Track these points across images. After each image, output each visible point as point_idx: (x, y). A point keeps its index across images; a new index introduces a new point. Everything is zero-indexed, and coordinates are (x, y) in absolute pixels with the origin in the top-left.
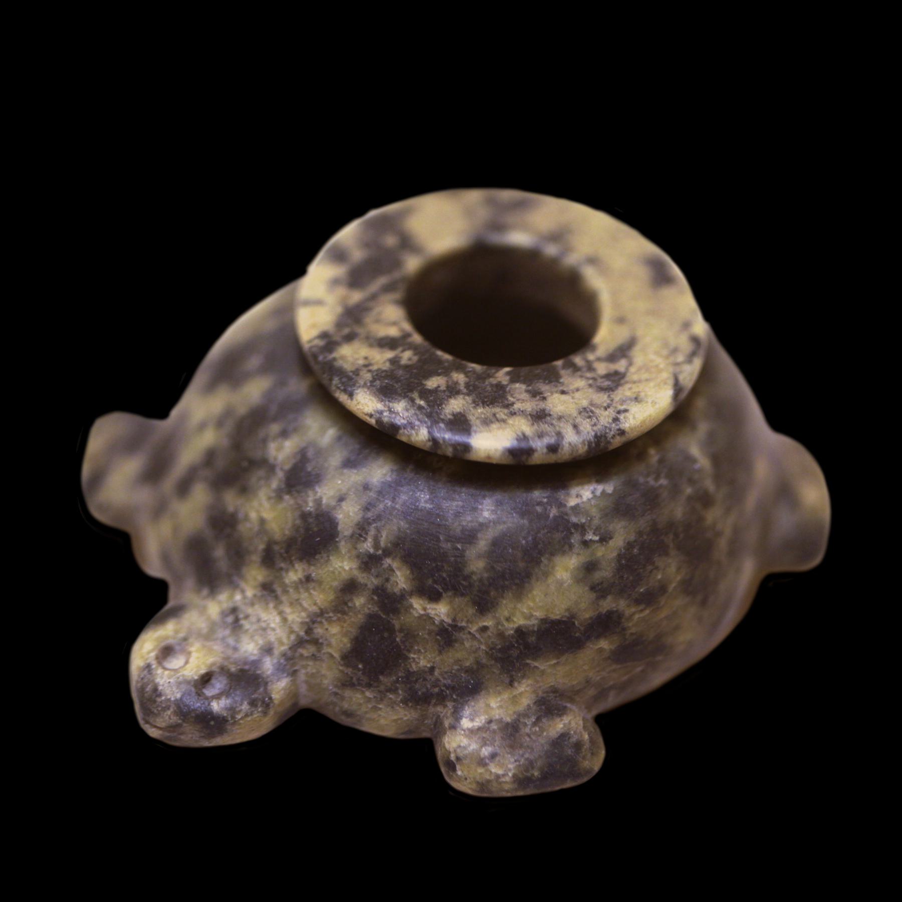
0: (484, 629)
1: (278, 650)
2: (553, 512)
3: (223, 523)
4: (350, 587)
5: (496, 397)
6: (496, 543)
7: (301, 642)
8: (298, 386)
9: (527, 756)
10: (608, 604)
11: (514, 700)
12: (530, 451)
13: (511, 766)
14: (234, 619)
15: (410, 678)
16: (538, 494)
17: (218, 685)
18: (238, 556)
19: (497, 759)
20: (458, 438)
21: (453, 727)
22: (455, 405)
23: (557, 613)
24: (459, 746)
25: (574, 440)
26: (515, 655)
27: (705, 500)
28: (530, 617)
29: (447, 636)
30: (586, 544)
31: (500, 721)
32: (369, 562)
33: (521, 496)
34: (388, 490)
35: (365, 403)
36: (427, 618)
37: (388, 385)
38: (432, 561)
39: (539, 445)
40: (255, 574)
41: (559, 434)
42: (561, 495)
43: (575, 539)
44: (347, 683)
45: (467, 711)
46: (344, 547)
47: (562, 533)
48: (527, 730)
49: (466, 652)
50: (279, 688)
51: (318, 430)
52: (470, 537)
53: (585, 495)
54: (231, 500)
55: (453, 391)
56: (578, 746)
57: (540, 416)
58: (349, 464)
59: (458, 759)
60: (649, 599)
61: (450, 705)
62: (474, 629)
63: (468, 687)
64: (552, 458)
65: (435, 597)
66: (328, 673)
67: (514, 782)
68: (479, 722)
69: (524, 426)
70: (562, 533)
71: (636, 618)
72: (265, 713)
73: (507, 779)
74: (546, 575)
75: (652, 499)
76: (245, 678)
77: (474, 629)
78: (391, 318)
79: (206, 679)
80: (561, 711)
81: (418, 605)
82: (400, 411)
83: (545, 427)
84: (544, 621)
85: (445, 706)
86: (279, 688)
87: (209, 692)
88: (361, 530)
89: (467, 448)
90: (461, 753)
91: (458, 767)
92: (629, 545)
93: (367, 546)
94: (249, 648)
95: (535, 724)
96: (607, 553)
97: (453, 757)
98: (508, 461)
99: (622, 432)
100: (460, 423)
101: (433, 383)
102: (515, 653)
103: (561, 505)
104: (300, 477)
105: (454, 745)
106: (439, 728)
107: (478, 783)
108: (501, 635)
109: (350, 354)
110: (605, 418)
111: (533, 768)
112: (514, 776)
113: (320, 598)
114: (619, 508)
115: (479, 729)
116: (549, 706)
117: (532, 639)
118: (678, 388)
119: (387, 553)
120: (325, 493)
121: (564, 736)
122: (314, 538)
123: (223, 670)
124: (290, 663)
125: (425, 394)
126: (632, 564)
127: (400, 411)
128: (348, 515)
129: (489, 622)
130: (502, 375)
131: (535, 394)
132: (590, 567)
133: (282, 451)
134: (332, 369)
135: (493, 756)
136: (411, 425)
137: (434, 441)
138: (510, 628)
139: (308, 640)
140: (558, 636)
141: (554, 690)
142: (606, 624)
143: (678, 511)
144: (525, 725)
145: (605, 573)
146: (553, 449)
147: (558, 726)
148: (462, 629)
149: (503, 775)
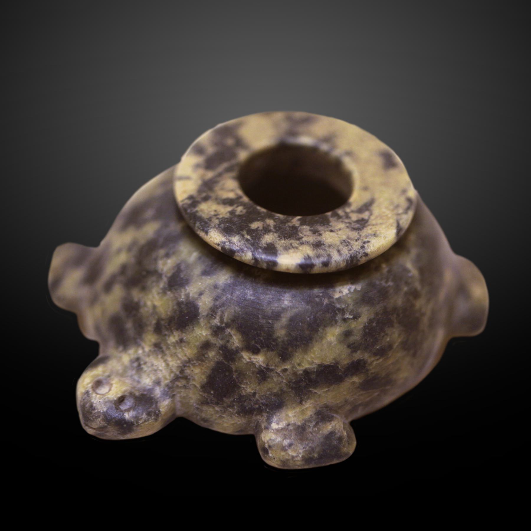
0: (285, 370)
1: (164, 383)
2: (326, 301)
3: (131, 308)
4: (206, 346)
5: (292, 234)
6: (292, 320)
7: (177, 378)
8: (175, 227)
9: (310, 445)
10: (358, 356)
11: (303, 412)
12: (312, 266)
13: (301, 451)
14: (138, 364)
15: (241, 399)
16: (317, 291)
17: (129, 403)
18: (140, 328)
19: (293, 447)
20: (270, 258)
21: (267, 428)
22: (268, 238)
23: (328, 361)
24: (270, 439)
25: (338, 259)
26: (303, 385)
27: (415, 294)
28: (312, 363)
29: (263, 374)
30: (345, 320)
31: (294, 424)
32: (217, 331)
33: (307, 292)
34: (229, 288)
35: (215, 237)
36: (252, 364)
37: (229, 227)
38: (255, 330)
39: (318, 262)
40: (150, 338)
41: (329, 256)
42: (330, 291)
43: (339, 317)
44: (204, 402)
45: (275, 419)
46: (202, 322)
47: (331, 314)
48: (310, 430)
49: (274, 384)
50: (164, 405)
51: (187, 253)
52: (277, 316)
53: (344, 291)
54: (136, 294)
55: (267, 230)
56: (340, 439)
57: (318, 245)
58: (206, 273)
59: (270, 447)
60: (382, 353)
61: (265, 415)
62: (279, 370)
63: (275, 405)
64: (325, 270)
65: (256, 351)
66: (193, 396)
67: (303, 460)
68: (282, 425)
69: (308, 251)
70: (331, 314)
71: (375, 364)
72: (156, 420)
73: (299, 459)
74: (322, 338)
75: (384, 294)
76: (144, 399)
77: (279, 370)
78: (230, 187)
79: (121, 400)
80: (330, 419)
81: (246, 356)
82: (236, 242)
83: (321, 251)
84: (320, 365)
85: (262, 416)
86: (164, 405)
87: (123, 407)
88: (213, 312)
89: (275, 264)
90: (271, 443)
91: (270, 451)
92: (371, 321)
93: (216, 321)
94: (147, 381)
95: (315, 426)
96: (358, 326)
97: (266, 446)
98: (299, 271)
99: (366, 255)
100: (271, 249)
101: (255, 225)
102: (303, 384)
103: (330, 297)
104: (177, 281)
105: (267, 438)
106: (258, 429)
107: (281, 461)
108: (295, 374)
109: (206, 209)
110: (356, 246)
111: (314, 452)
112: (303, 457)
113: (189, 352)
114: (365, 299)
115: (282, 429)
116: (323, 415)
117: (313, 376)
118: (399, 229)
119: (228, 325)
120: (192, 290)
121: (332, 433)
122: (185, 316)
123: (131, 394)
124: (170, 390)
125: (250, 232)
126: (372, 332)
127: (236, 242)
128: (205, 303)
129: (288, 366)
130: (296, 221)
131: (315, 232)
132: (347, 334)
133: (166, 266)
134: (195, 217)
135: (290, 445)
136: (242, 250)
137: (256, 259)
138: (300, 370)
139: (181, 377)
140: (329, 374)
141: (326, 406)
142: (357, 367)
143: (399, 301)
144: (309, 427)
145: (356, 337)
146: (326, 264)
147: (328, 427)
148: (272, 370)
149: (296, 456)
